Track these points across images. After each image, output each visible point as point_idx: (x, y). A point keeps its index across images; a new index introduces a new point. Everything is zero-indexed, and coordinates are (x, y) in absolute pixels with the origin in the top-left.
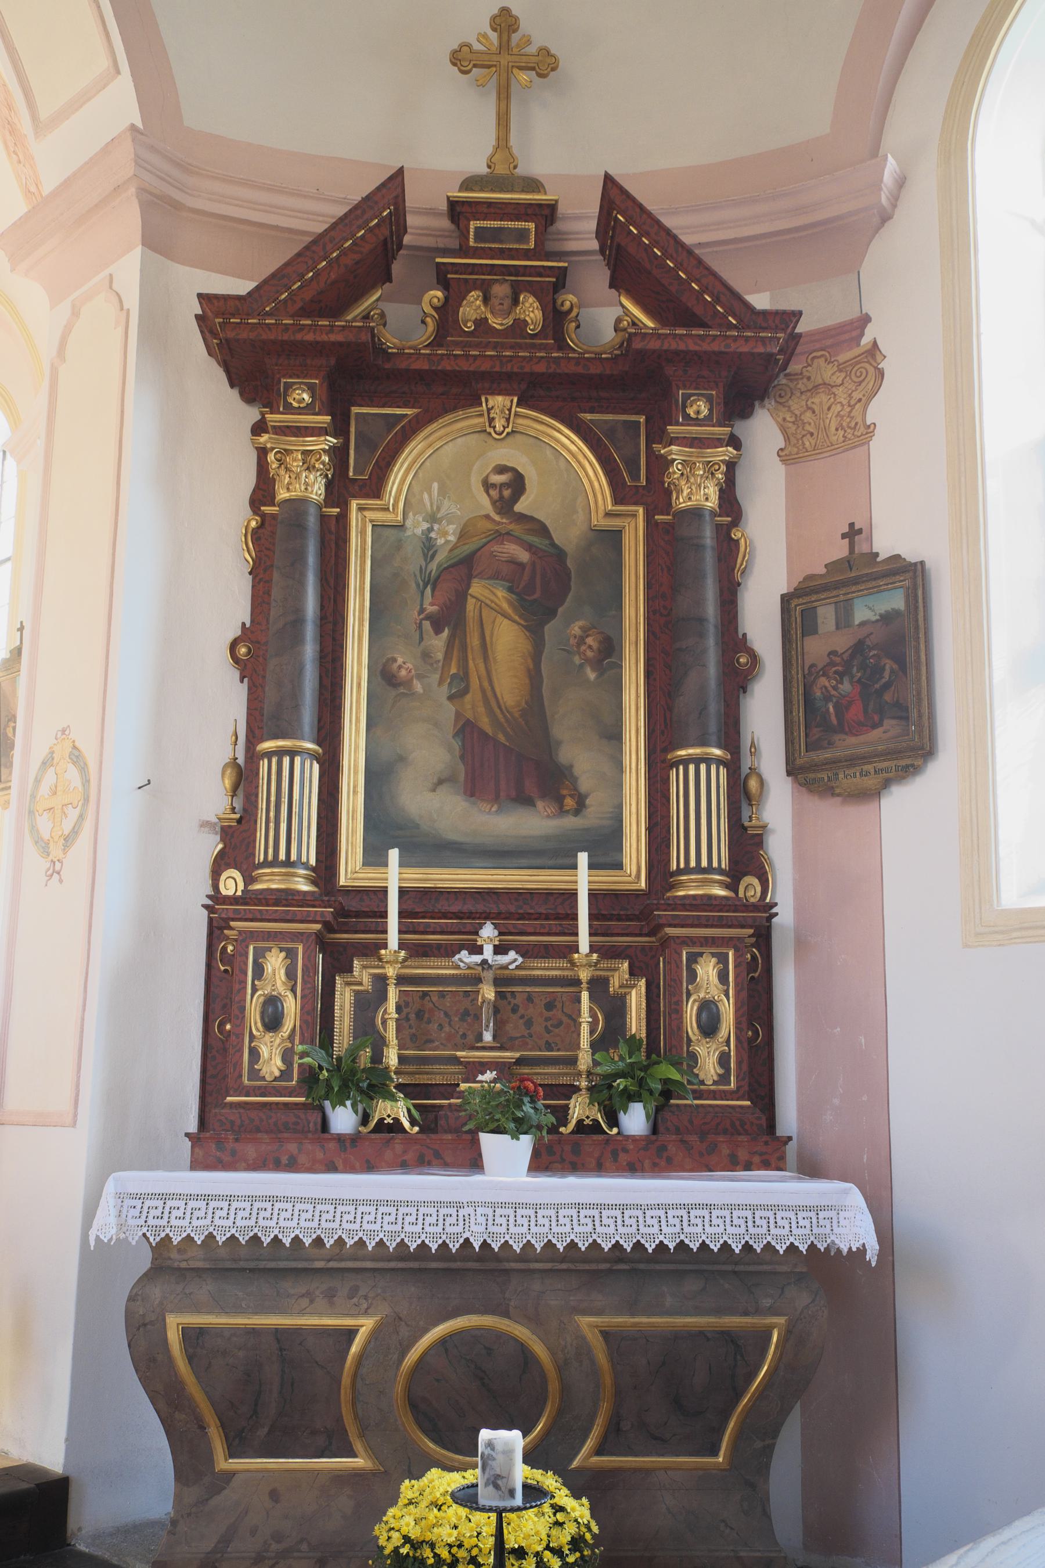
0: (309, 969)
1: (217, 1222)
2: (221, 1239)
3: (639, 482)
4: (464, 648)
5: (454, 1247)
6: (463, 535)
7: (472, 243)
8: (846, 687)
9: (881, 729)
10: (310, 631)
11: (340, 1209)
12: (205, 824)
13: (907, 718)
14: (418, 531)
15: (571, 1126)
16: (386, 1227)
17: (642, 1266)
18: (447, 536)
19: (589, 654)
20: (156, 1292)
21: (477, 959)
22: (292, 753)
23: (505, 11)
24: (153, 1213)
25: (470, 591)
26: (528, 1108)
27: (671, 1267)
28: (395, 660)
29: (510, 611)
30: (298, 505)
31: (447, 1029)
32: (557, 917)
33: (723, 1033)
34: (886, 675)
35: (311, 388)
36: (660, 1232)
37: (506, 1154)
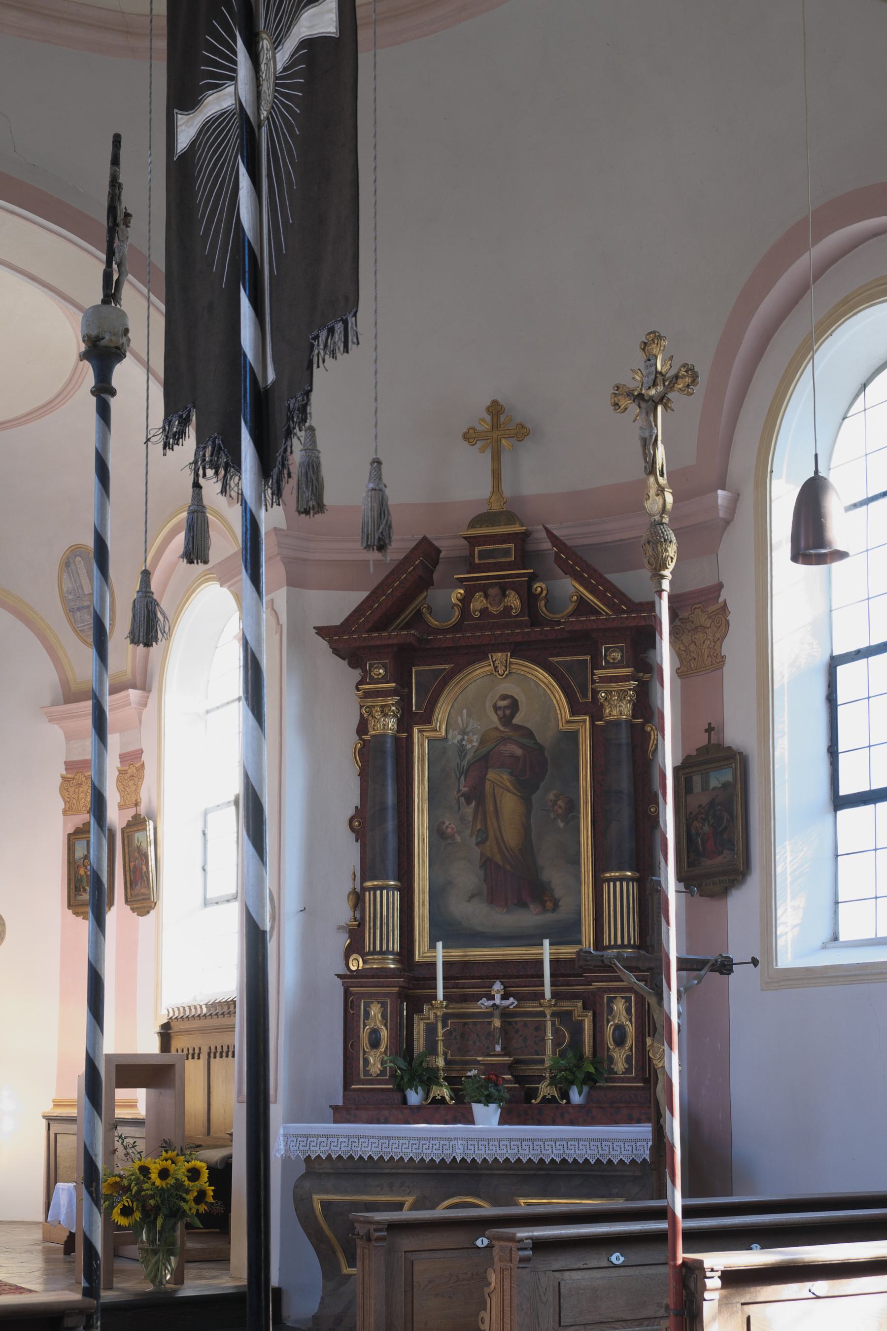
0: (397, 1012)
1: (332, 1148)
2: (334, 1157)
3: (583, 702)
4: (485, 813)
5: (448, 1161)
6: (482, 742)
7: (477, 561)
8: (706, 828)
9: (722, 856)
10: (390, 814)
11: (391, 1141)
12: (340, 928)
13: (733, 850)
14: (456, 741)
15: (539, 1100)
16: (414, 1151)
17: (552, 1172)
18: (473, 742)
19: (560, 811)
20: (307, 1184)
21: (491, 1003)
22: (381, 889)
23: (495, 403)
24: (302, 1144)
25: (488, 777)
26: (492, 1090)
27: (568, 1173)
28: (444, 823)
29: (511, 787)
30: (380, 738)
31: (478, 1043)
32: (532, 976)
33: (628, 1044)
34: (725, 822)
35: (384, 666)
36: (553, 1153)
37: (487, 1117)
